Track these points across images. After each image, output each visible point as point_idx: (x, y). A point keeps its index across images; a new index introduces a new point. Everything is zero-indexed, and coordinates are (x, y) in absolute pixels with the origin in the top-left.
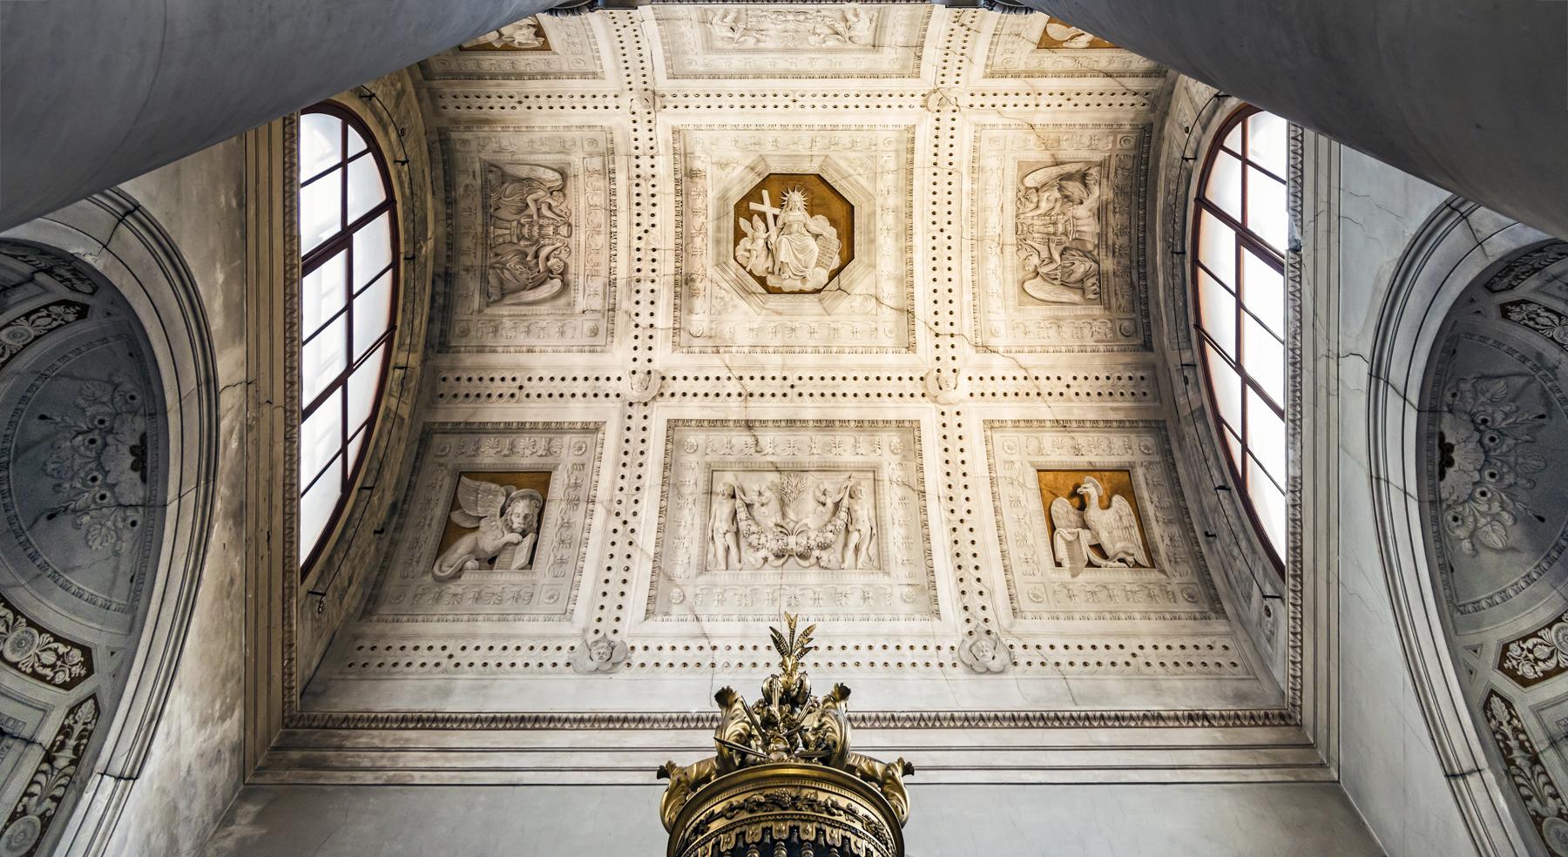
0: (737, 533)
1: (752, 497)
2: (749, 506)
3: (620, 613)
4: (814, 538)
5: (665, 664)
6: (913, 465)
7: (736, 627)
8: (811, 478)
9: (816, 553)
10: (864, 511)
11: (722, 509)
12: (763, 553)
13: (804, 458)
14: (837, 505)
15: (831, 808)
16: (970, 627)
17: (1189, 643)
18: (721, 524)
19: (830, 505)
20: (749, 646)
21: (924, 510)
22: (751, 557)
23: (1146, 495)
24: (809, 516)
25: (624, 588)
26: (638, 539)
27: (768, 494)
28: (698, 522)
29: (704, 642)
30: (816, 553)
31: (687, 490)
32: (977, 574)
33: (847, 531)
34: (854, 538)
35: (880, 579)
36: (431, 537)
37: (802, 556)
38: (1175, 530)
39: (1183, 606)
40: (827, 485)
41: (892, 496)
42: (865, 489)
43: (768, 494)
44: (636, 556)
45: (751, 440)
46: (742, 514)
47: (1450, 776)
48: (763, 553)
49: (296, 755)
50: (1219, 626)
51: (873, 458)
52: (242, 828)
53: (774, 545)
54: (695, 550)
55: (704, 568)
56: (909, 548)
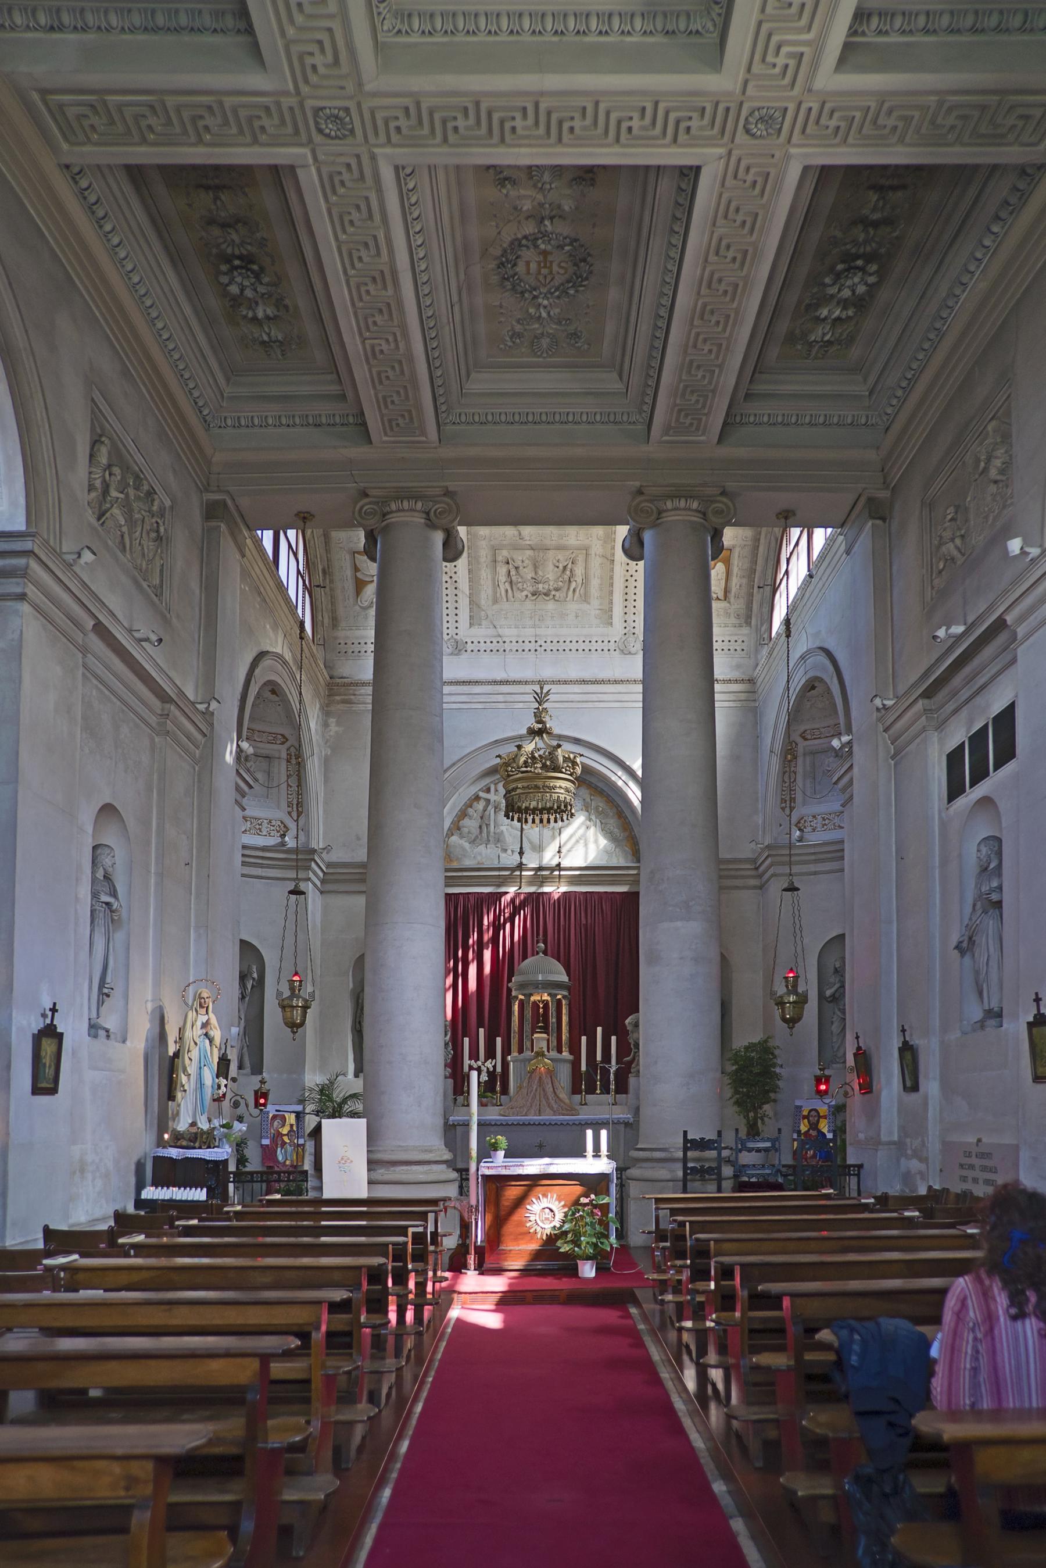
0: (511, 582)
1: (519, 563)
2: (517, 568)
3: (457, 612)
4: (552, 585)
5: (482, 651)
6: (609, 546)
7: (514, 631)
8: (551, 553)
9: (553, 593)
10: (579, 571)
11: (502, 570)
12: (525, 593)
13: (547, 542)
14: (565, 568)
15: (554, 788)
16: (625, 631)
17: (726, 639)
18: (503, 578)
19: (561, 567)
20: (520, 641)
21: (612, 570)
22: (518, 594)
23: (736, 563)
24: (550, 573)
25: (457, 625)
26: (460, 585)
27: (527, 562)
28: (489, 577)
29: (499, 639)
30: (553, 593)
31: (482, 560)
32: (634, 604)
33: (570, 581)
34: (573, 585)
35: (585, 606)
36: (350, 586)
37: (546, 595)
38: (744, 581)
39: (733, 620)
40: (560, 557)
41: (595, 563)
42: (581, 559)
43: (527, 562)
44: (460, 595)
45: (516, 533)
46: (513, 572)
47: (771, 752)
48: (525, 593)
49: (338, 698)
50: (745, 630)
51: (587, 542)
52: (334, 728)
53: (531, 589)
54: (490, 592)
55: (495, 601)
56: (601, 590)
